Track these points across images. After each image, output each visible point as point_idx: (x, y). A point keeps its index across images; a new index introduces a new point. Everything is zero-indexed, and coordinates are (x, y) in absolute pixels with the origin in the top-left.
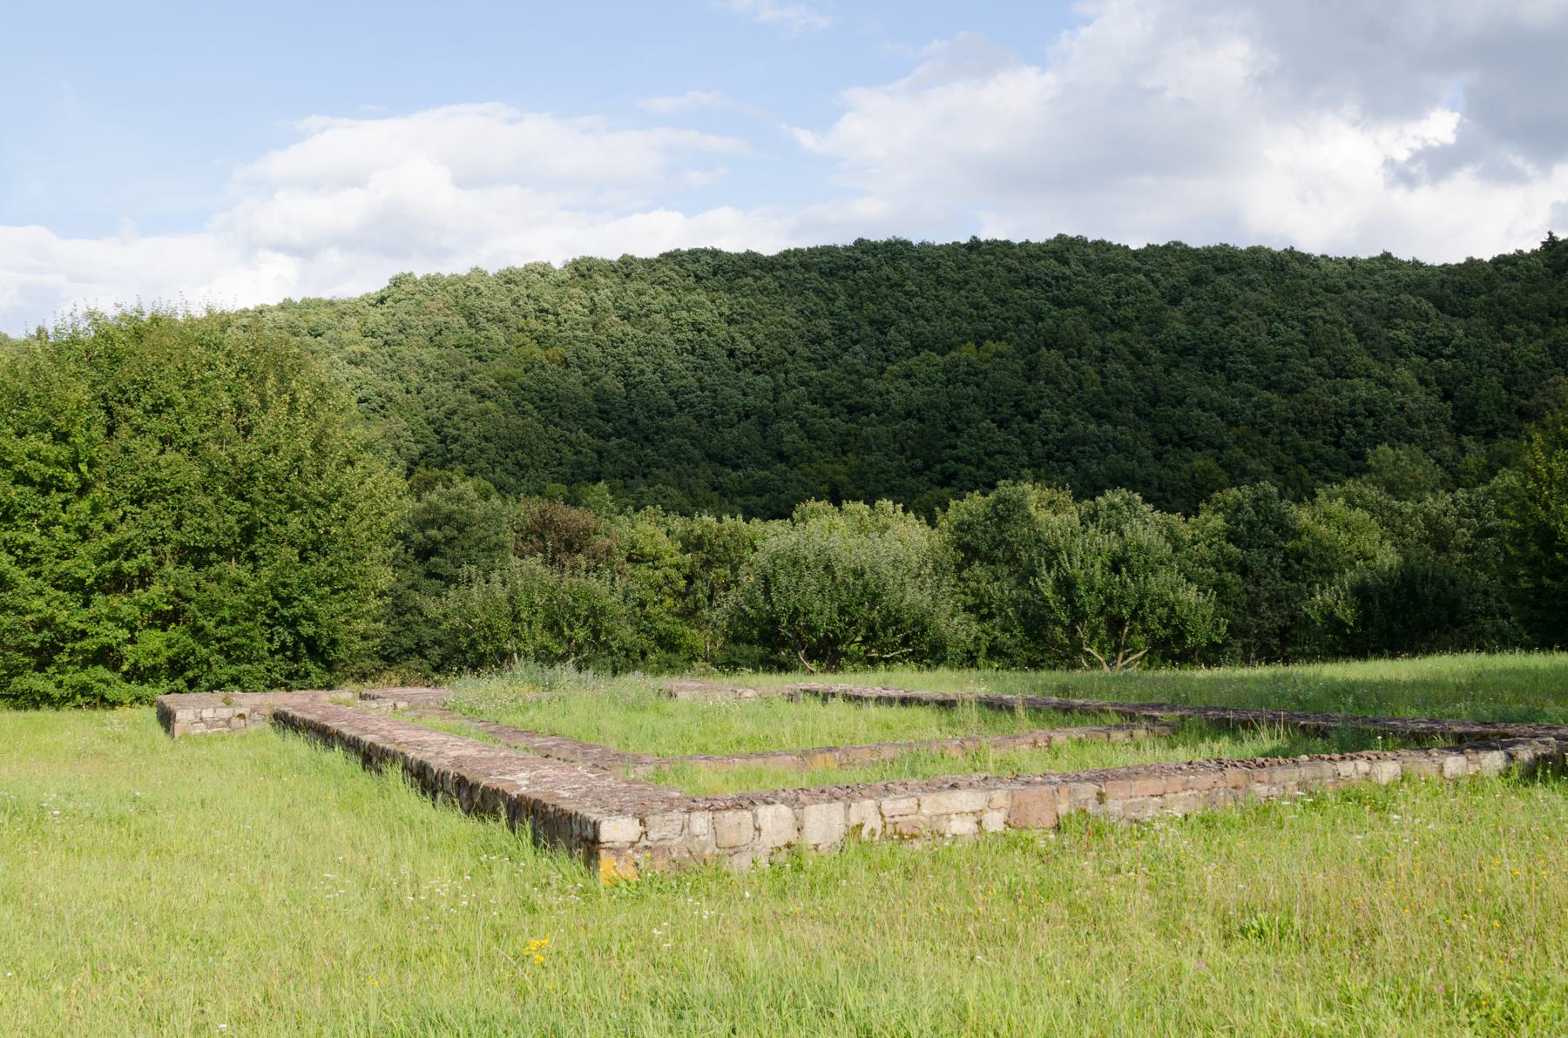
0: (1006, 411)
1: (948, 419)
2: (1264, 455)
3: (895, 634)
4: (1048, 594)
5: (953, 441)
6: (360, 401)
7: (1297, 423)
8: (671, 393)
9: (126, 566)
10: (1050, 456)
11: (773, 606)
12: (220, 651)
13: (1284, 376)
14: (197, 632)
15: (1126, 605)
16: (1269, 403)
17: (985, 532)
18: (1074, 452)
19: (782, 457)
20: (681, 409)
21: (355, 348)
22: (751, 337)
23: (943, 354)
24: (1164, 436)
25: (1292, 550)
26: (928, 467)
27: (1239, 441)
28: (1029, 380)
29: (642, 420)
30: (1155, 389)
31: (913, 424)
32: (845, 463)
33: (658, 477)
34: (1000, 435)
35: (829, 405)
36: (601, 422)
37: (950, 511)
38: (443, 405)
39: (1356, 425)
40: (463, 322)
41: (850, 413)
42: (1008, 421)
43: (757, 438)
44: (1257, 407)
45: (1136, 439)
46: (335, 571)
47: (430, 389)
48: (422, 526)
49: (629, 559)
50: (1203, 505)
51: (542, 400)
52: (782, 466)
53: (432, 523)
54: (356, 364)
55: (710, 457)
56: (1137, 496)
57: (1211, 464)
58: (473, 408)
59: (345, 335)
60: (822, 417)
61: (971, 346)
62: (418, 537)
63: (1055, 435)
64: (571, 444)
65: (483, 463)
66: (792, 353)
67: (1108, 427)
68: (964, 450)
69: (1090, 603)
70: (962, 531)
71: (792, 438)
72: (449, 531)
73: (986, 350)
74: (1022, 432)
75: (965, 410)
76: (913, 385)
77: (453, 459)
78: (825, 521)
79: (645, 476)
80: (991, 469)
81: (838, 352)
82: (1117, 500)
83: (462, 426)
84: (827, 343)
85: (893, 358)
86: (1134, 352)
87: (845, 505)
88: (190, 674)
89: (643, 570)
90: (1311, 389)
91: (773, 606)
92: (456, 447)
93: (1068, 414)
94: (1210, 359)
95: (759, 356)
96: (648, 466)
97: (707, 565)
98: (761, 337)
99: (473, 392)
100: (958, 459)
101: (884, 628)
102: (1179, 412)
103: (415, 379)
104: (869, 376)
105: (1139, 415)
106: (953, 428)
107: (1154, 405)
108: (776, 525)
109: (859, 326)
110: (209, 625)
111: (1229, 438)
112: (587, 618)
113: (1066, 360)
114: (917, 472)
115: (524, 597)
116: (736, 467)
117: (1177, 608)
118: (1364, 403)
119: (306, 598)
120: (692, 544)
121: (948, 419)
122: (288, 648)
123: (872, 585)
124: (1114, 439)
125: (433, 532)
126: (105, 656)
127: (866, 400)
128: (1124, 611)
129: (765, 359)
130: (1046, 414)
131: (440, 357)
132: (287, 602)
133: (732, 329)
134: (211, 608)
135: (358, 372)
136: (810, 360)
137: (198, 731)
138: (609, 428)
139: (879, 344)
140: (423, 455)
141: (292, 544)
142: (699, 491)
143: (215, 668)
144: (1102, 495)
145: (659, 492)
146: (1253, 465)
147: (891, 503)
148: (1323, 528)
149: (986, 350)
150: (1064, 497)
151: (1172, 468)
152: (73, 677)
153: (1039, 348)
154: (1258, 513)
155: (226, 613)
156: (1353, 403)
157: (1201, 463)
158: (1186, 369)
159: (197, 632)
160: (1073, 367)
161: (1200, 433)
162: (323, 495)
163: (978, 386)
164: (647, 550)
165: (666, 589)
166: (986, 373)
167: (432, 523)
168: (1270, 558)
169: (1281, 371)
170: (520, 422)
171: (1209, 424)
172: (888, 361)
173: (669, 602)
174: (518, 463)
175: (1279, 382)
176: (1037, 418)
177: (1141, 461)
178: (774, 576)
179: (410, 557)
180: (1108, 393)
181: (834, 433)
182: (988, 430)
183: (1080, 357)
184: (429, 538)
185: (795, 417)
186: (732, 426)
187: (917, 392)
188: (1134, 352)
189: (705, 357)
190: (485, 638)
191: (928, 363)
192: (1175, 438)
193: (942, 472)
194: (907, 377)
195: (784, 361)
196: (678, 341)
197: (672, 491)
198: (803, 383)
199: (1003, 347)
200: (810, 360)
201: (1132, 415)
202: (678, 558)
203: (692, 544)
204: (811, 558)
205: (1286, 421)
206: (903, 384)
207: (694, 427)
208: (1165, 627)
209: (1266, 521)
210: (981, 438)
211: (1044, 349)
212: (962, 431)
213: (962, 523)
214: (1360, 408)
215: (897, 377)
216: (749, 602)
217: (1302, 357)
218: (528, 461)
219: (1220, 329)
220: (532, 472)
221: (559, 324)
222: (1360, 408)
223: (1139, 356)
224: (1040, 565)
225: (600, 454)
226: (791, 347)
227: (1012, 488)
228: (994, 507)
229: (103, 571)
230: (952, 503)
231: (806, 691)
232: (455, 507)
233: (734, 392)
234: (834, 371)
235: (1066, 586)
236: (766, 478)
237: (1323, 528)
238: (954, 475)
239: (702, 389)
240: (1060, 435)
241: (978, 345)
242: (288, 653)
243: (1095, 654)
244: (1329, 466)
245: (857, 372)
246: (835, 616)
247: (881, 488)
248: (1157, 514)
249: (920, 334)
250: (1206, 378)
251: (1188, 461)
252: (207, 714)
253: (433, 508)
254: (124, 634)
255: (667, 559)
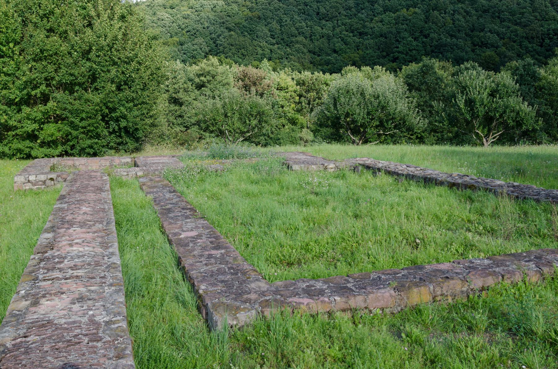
0: (417, 34)
1: (396, 37)
2: (514, 50)
3: (391, 124)
4: (462, 106)
5: (398, 45)
6: (187, 32)
7: (527, 38)
8: (297, 28)
9: (33, 93)
10: (432, 51)
11: (338, 111)
12: (84, 133)
13: (522, 20)
14: (72, 125)
15: (498, 112)
16: (516, 31)
17: (418, 78)
18: (442, 50)
19: (335, 51)
20: (299, 34)
21: (185, 12)
22: (325, 8)
23: (394, 13)
24: (476, 43)
25: (538, 86)
26: (388, 55)
27: (504, 45)
28: (426, 23)
29: (285, 38)
30: (473, 26)
31: (383, 39)
32: (358, 53)
33: (291, 59)
34: (415, 43)
35: (352, 32)
36: (271, 39)
37: (403, 70)
38: (216, 33)
39: (550, 38)
40: (223, 3)
41: (360, 35)
42: (417, 38)
43: (327, 45)
44: (512, 32)
45: (465, 44)
46: (134, 95)
47: (212, 28)
48: (199, 76)
49: (277, 89)
50: (502, 68)
51: (251, 31)
52: (336, 55)
53: (202, 75)
54: (186, 19)
55: (310, 51)
56: (476, 64)
57: (493, 53)
58: (227, 34)
59: (182, 8)
60: (350, 37)
61: (405, 10)
62: (197, 80)
63: (435, 43)
64: (261, 47)
65: (230, 54)
66: (339, 13)
67: (454, 40)
68: (401, 48)
69: (481, 111)
70: (408, 78)
71: (339, 45)
72: (208, 78)
73: (410, 11)
74: (423, 42)
75: (402, 34)
76: (383, 25)
77: (220, 52)
78: (354, 74)
79: (287, 58)
80: (411, 56)
81: (356, 13)
82: (469, 66)
83: (223, 40)
84: (353, 9)
85: (376, 15)
86: (465, 11)
87: (362, 68)
88: (71, 144)
89: (282, 93)
90: (533, 25)
91: (338, 111)
92: (221, 48)
93: (440, 35)
94: (494, 14)
95: (328, 15)
96: (288, 55)
97: (308, 91)
98: (328, 7)
99: (226, 28)
100: (399, 52)
101: (387, 121)
102: (482, 34)
103: (206, 25)
104: (368, 21)
105: (467, 36)
106: (397, 41)
107: (472, 31)
108: (334, 75)
109: (364, 3)
110: (77, 121)
111: (500, 43)
112: (256, 116)
113: (440, 15)
114: (384, 57)
115: (229, 106)
116: (319, 56)
117: (521, 113)
118: (553, 30)
119: (122, 108)
120: (300, 83)
121: (396, 37)
122: (117, 132)
123: (383, 102)
124: (457, 44)
125: (202, 78)
126: (32, 137)
127: (366, 30)
128: (497, 115)
129: (330, 16)
130: (432, 35)
131: (215, 16)
132: (113, 110)
133: (318, 4)
134: (76, 113)
135: (187, 21)
136: (346, 16)
137: (27, 188)
138: (274, 41)
139: (371, 9)
140: (210, 51)
141: (112, 82)
142: (305, 64)
143: (81, 141)
144: (463, 64)
145: (292, 64)
146: (509, 54)
147: (381, 67)
148: (551, 77)
149: (410, 11)
150: (447, 64)
151: (478, 55)
152: (17, 145)
153: (430, 10)
154: (525, 71)
155: (84, 115)
156: (548, 30)
157: (489, 53)
158: (485, 18)
159: (72, 125)
160: (443, 17)
161: (489, 42)
162: (128, 58)
163: (407, 25)
164: (282, 85)
165: (292, 100)
166: (410, 20)
167: (202, 75)
168: (529, 89)
169: (521, 18)
170: (244, 39)
171: (494, 38)
172: (374, 16)
173: (293, 105)
174: (242, 54)
175: (520, 22)
176: (429, 37)
177: (467, 52)
178: (338, 98)
179: (194, 88)
180: (455, 27)
181: (354, 42)
182: (410, 41)
183: (445, 14)
184: (201, 80)
185: (340, 37)
186: (317, 40)
187: (385, 27)
188: (465, 11)
189: (308, 15)
190: (213, 124)
191: (389, 17)
192: (480, 44)
193: (393, 57)
194: (381, 22)
195: (337, 16)
196: (299, 9)
197: (296, 64)
198: (343, 24)
199: (417, 10)
200: (346, 16)
201: (464, 35)
202: (295, 87)
203: (300, 83)
204: (355, 90)
205: (523, 37)
206: (380, 24)
207: (304, 41)
208: (513, 121)
209: (528, 74)
210: (408, 44)
211: (431, 11)
212: (401, 42)
213: (409, 75)
214: (551, 32)
215: (377, 22)
216: (327, 109)
217: (530, 13)
218: (246, 53)
219: (499, 3)
220: (247, 57)
221: (257, 3)
222: (551, 32)
223: (467, 13)
224: (458, 93)
225: (271, 51)
226: (339, 11)
227: (429, 61)
228: (422, 69)
229: (22, 95)
230: (404, 67)
231: (363, 165)
232: (210, 69)
233: (319, 28)
234: (355, 20)
235: (470, 103)
236: (329, 59)
237: (551, 77)
238: (397, 58)
239: (307, 27)
240: (437, 43)
241: (407, 10)
242: (118, 134)
243: (480, 133)
244: (538, 54)
245: (363, 20)
246: (365, 116)
247: (371, 63)
248: (483, 71)
249: (387, 6)
250: (492, 21)
251: (484, 52)
252: (32, 178)
253: (202, 69)
254: (36, 126)
255: (290, 89)
